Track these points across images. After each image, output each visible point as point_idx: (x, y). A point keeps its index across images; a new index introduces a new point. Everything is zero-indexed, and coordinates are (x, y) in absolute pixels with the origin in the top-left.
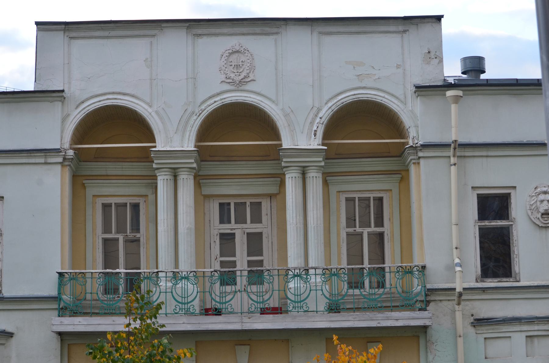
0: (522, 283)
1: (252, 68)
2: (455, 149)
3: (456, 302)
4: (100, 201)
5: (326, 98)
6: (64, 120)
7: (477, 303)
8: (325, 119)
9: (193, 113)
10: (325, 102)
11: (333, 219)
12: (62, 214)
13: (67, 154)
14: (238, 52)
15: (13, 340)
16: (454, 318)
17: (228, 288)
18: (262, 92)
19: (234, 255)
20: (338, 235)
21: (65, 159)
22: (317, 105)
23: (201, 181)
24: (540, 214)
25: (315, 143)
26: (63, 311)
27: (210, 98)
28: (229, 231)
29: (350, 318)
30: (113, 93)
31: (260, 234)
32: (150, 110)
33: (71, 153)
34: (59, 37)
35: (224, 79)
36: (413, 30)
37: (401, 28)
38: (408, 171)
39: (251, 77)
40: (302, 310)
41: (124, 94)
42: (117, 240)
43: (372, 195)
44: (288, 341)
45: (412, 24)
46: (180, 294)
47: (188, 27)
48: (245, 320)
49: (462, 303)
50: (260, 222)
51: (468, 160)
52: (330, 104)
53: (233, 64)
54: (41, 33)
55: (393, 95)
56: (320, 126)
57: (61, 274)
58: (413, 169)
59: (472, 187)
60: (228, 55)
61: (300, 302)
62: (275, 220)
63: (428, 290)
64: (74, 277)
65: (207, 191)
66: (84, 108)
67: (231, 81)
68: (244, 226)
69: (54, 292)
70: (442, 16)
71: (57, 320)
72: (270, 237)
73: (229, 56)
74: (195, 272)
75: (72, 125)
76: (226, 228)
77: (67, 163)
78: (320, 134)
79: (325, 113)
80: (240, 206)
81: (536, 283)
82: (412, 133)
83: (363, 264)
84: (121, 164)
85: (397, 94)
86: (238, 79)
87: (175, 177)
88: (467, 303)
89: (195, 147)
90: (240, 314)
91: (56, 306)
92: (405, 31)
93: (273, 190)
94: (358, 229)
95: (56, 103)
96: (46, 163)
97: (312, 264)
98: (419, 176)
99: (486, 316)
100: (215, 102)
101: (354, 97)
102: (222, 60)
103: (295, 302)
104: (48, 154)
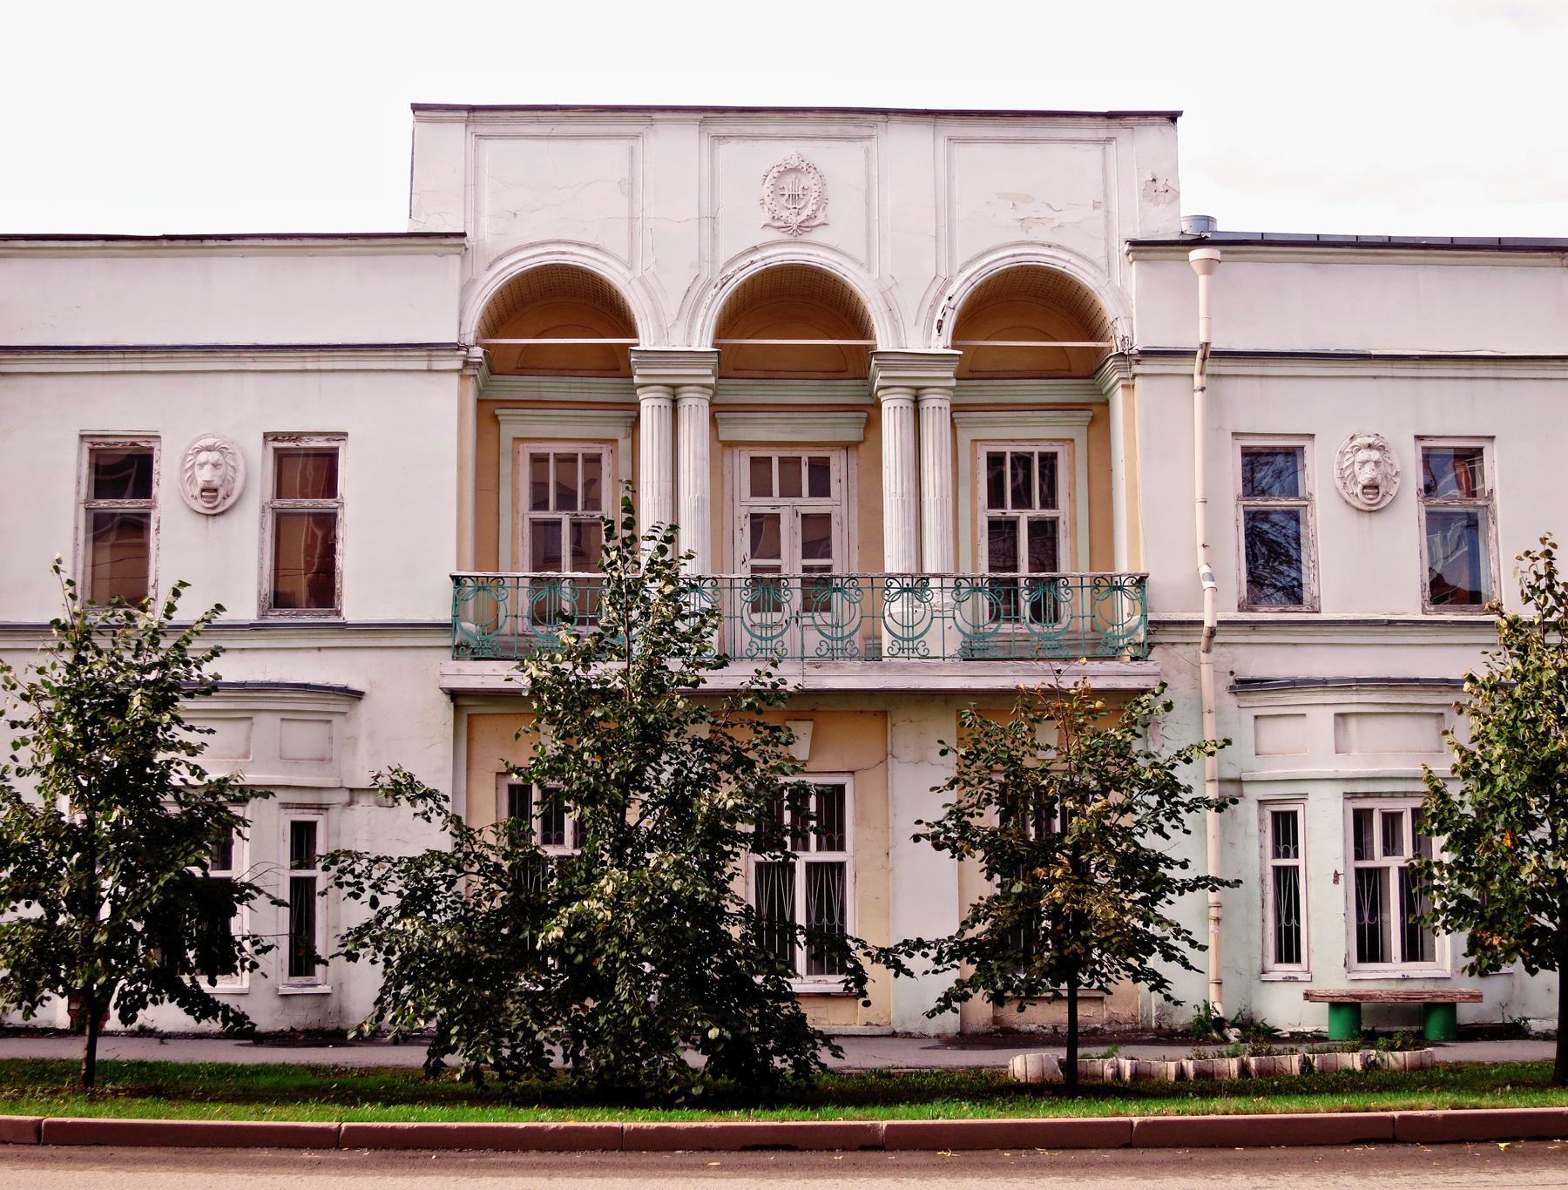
0: (1324, 616)
1: (823, 201)
2: (1204, 359)
3: (1203, 646)
4: (526, 450)
5: (959, 262)
6: (466, 288)
7: (1241, 650)
8: (959, 301)
9: (711, 282)
10: (958, 268)
11: (964, 492)
12: (460, 468)
13: (471, 355)
14: (796, 170)
15: (363, 706)
16: (1197, 678)
17: (756, 617)
18: (840, 248)
19: (778, 556)
20: (974, 521)
21: (466, 363)
22: (943, 273)
23: (717, 415)
24: (1360, 487)
25: (940, 344)
26: (462, 650)
27: (743, 255)
28: (769, 511)
29: (1008, 671)
30: (559, 242)
31: (827, 517)
32: (628, 275)
33: (478, 352)
34: (454, 134)
35: (768, 221)
36: (1121, 134)
37: (1103, 134)
38: (1107, 404)
39: (821, 218)
40: (916, 655)
41: (581, 245)
42: (558, 523)
43: (1036, 450)
44: (884, 714)
45: (1124, 127)
46: (898, 618)
47: (701, 121)
48: (810, 670)
49: (1215, 649)
50: (826, 493)
51: (1225, 382)
52: (967, 273)
53: (787, 193)
54: (421, 126)
55: (1085, 258)
56: (949, 312)
57: (457, 580)
58: (1119, 399)
59: (1233, 434)
60: (776, 175)
61: (909, 640)
62: (854, 491)
63: (1151, 623)
64: (482, 585)
65: (727, 434)
66: (503, 270)
67: (782, 224)
68: (797, 501)
69: (446, 617)
70: (1180, 113)
71: (452, 666)
72: (845, 524)
73: (779, 178)
74: (714, 578)
75: (479, 300)
76: (763, 505)
77: (469, 372)
78: (948, 327)
79: (960, 290)
80: (790, 464)
81: (1351, 617)
82: (1121, 330)
83: (1055, 570)
84: (568, 379)
85: (1093, 257)
86: (795, 220)
87: (917, 402)
88: (1223, 649)
89: (714, 345)
90: (798, 660)
91: (449, 642)
92: (1109, 140)
93: (852, 434)
94: (1010, 512)
95: (451, 257)
96: (430, 371)
97: (930, 568)
98: (1130, 410)
99: (1258, 675)
100: (752, 262)
101: (1014, 259)
102: (766, 185)
103: (903, 639)
104: (435, 353)
